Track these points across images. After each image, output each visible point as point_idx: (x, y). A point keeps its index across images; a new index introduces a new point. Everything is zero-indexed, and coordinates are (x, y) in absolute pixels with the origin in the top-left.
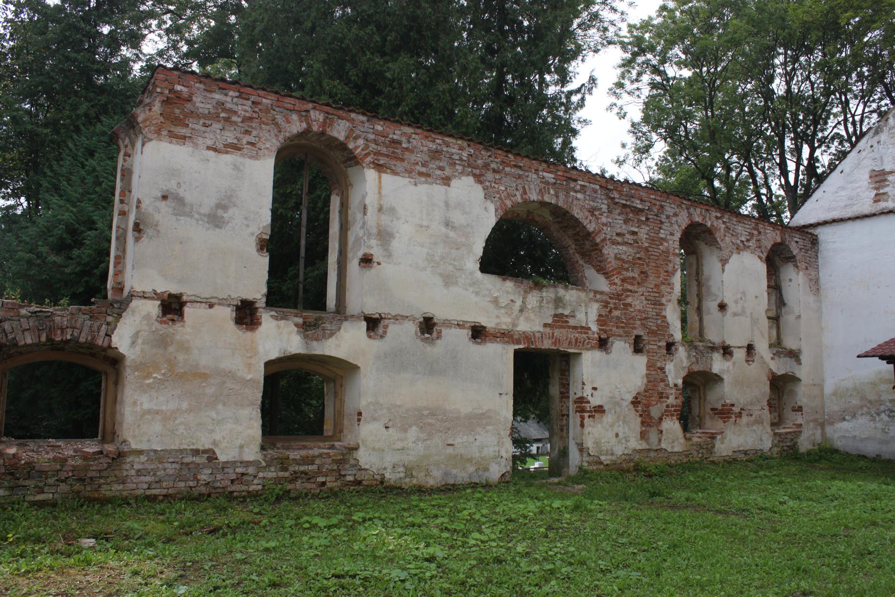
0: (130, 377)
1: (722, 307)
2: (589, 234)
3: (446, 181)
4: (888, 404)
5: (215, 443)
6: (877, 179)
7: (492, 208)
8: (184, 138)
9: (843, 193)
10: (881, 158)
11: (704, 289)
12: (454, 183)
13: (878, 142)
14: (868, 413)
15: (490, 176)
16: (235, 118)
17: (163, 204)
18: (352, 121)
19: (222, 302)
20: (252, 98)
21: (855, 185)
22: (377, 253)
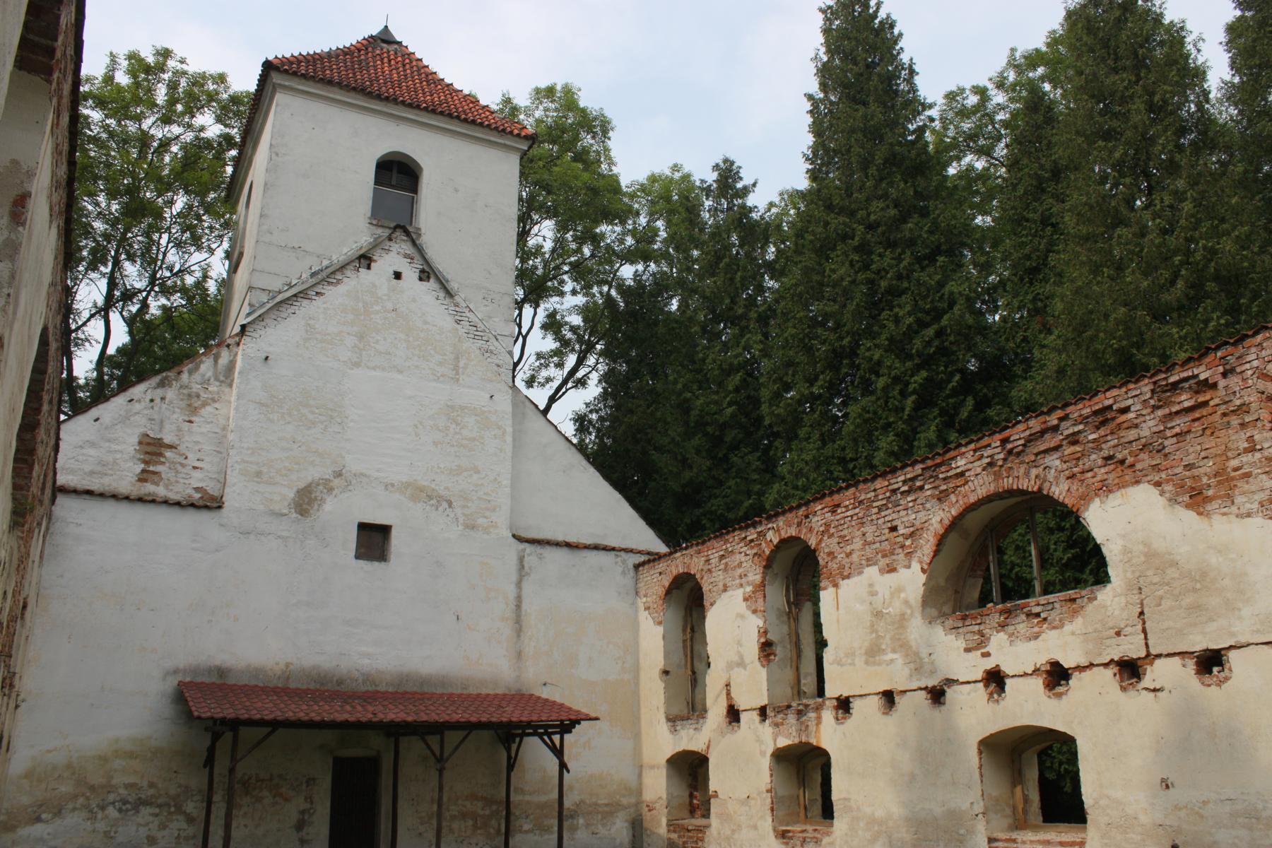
4: (122, 791)
6: (149, 449)
9: (92, 452)
10: (162, 422)
13: (163, 399)
14: (87, 807)
21: (114, 447)
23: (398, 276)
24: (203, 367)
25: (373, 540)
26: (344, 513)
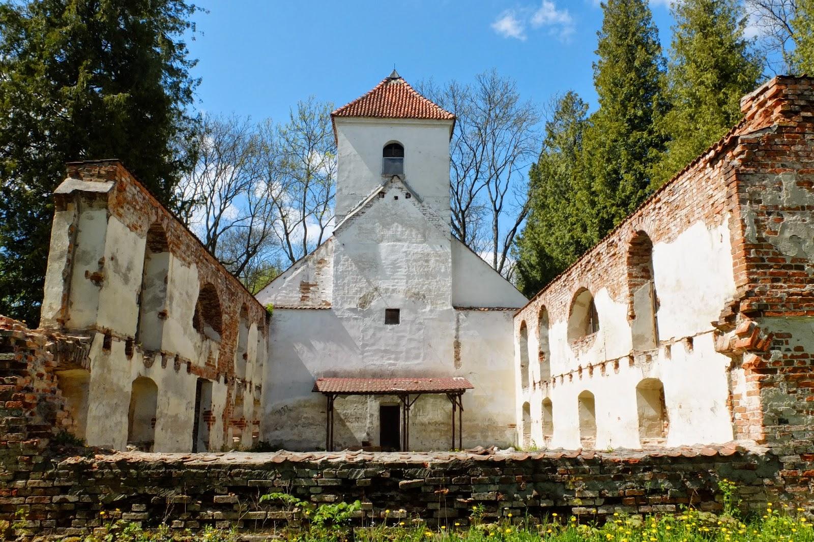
0: (93, 393)
6: (304, 287)
17: (111, 263)
23: (396, 198)
24: (322, 250)
25: (392, 316)
26: (379, 305)
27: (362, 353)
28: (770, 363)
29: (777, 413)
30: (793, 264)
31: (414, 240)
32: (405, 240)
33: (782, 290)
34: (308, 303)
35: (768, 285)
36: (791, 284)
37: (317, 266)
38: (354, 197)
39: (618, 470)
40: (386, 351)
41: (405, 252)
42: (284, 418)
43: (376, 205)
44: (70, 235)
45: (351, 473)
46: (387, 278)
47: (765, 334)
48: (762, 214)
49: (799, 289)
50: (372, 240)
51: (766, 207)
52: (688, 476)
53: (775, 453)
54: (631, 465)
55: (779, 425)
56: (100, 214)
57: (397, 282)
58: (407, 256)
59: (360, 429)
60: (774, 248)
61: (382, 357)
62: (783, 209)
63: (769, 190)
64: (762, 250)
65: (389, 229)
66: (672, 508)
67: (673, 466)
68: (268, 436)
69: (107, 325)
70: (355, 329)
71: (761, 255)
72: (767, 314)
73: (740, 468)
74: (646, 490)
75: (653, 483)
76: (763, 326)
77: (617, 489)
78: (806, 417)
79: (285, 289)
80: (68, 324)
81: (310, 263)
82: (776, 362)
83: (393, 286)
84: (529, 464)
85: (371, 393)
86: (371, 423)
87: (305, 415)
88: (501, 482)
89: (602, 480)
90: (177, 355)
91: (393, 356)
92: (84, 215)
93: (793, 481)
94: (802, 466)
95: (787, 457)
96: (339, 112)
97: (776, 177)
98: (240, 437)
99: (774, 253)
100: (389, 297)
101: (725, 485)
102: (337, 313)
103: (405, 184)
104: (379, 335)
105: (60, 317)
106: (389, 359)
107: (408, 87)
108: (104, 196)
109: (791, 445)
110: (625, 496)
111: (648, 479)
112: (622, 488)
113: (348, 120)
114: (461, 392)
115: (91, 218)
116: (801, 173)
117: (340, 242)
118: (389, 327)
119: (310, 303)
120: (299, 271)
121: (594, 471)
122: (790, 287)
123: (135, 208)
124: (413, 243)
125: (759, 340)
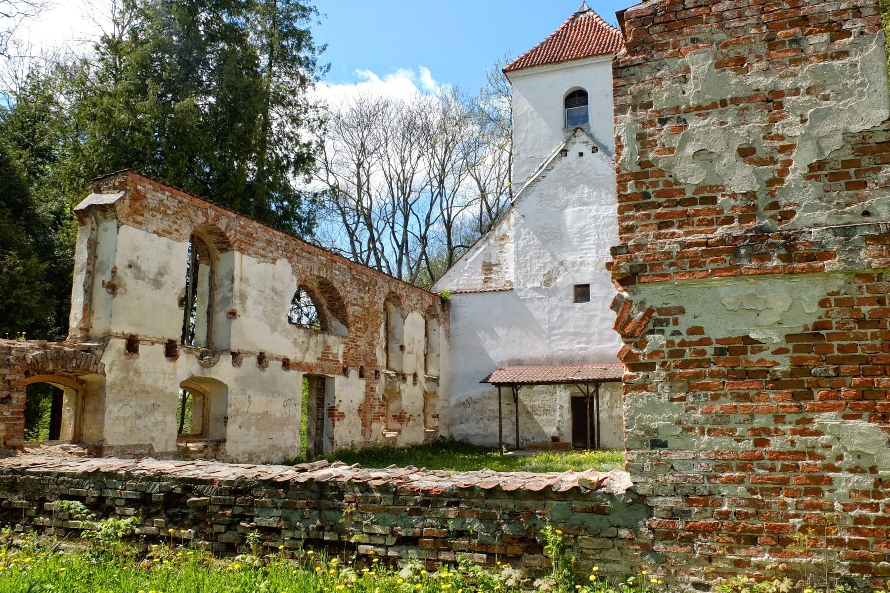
0: (110, 396)
1: (402, 348)
2: (340, 298)
3: (274, 261)
5: (152, 439)
7: (295, 279)
8: (141, 223)
11: (390, 335)
12: (278, 262)
15: (295, 258)
16: (169, 212)
17: (128, 271)
18: (229, 217)
19: (158, 342)
20: (178, 197)
22: (238, 308)
23: (581, 154)
26: (566, 281)
27: (549, 338)
28: (644, 355)
29: (649, 431)
30: (698, 197)
31: (603, 202)
32: (592, 203)
33: (675, 239)
34: (491, 285)
35: (651, 233)
36: (691, 229)
37: (499, 243)
38: (532, 160)
39: (416, 503)
40: (575, 334)
41: (594, 217)
42: (469, 411)
43: (558, 165)
44: (89, 248)
45: (148, 487)
46: (574, 250)
47: (639, 310)
48: (651, 123)
49: (703, 236)
50: (555, 207)
51: (658, 112)
52: (506, 517)
53: (641, 491)
54: (431, 496)
55: (652, 448)
56: (112, 225)
57: (586, 253)
58: (595, 221)
59: (549, 423)
60: (666, 174)
61: (571, 341)
62: (688, 110)
63: (666, 83)
64: (646, 181)
65: (574, 193)
66: (482, 558)
67: (487, 501)
68: (453, 430)
69: (129, 330)
70: (540, 311)
71: (644, 189)
72: (643, 279)
73: (584, 511)
74: (449, 531)
75: (459, 524)
76: (637, 299)
77: (412, 526)
78: (698, 439)
79: (467, 271)
80: (91, 332)
81: (492, 241)
82: (655, 353)
83: (581, 258)
84: (314, 487)
85: (559, 383)
86: (561, 415)
87: (490, 408)
88: (284, 506)
89: (397, 513)
90: (261, 353)
91: (584, 339)
92: (101, 227)
93: (668, 536)
94: (687, 514)
95: (660, 499)
96: (511, 66)
97: (680, 60)
98: (399, 431)
99: (667, 183)
100: (577, 271)
101: (551, 535)
102: (519, 294)
103: (591, 136)
104: (566, 316)
105: (82, 325)
106: (579, 343)
107: (598, 19)
108: (112, 206)
109: (669, 481)
110: (421, 536)
111: (452, 516)
112: (417, 525)
113: (537, 69)
114: (426, 393)
115: (106, 230)
116: (725, 46)
117: (519, 213)
118: (579, 305)
119: (493, 285)
120: (481, 250)
121: (388, 500)
122: (687, 234)
123: (165, 213)
124: (603, 205)
125: (630, 319)
